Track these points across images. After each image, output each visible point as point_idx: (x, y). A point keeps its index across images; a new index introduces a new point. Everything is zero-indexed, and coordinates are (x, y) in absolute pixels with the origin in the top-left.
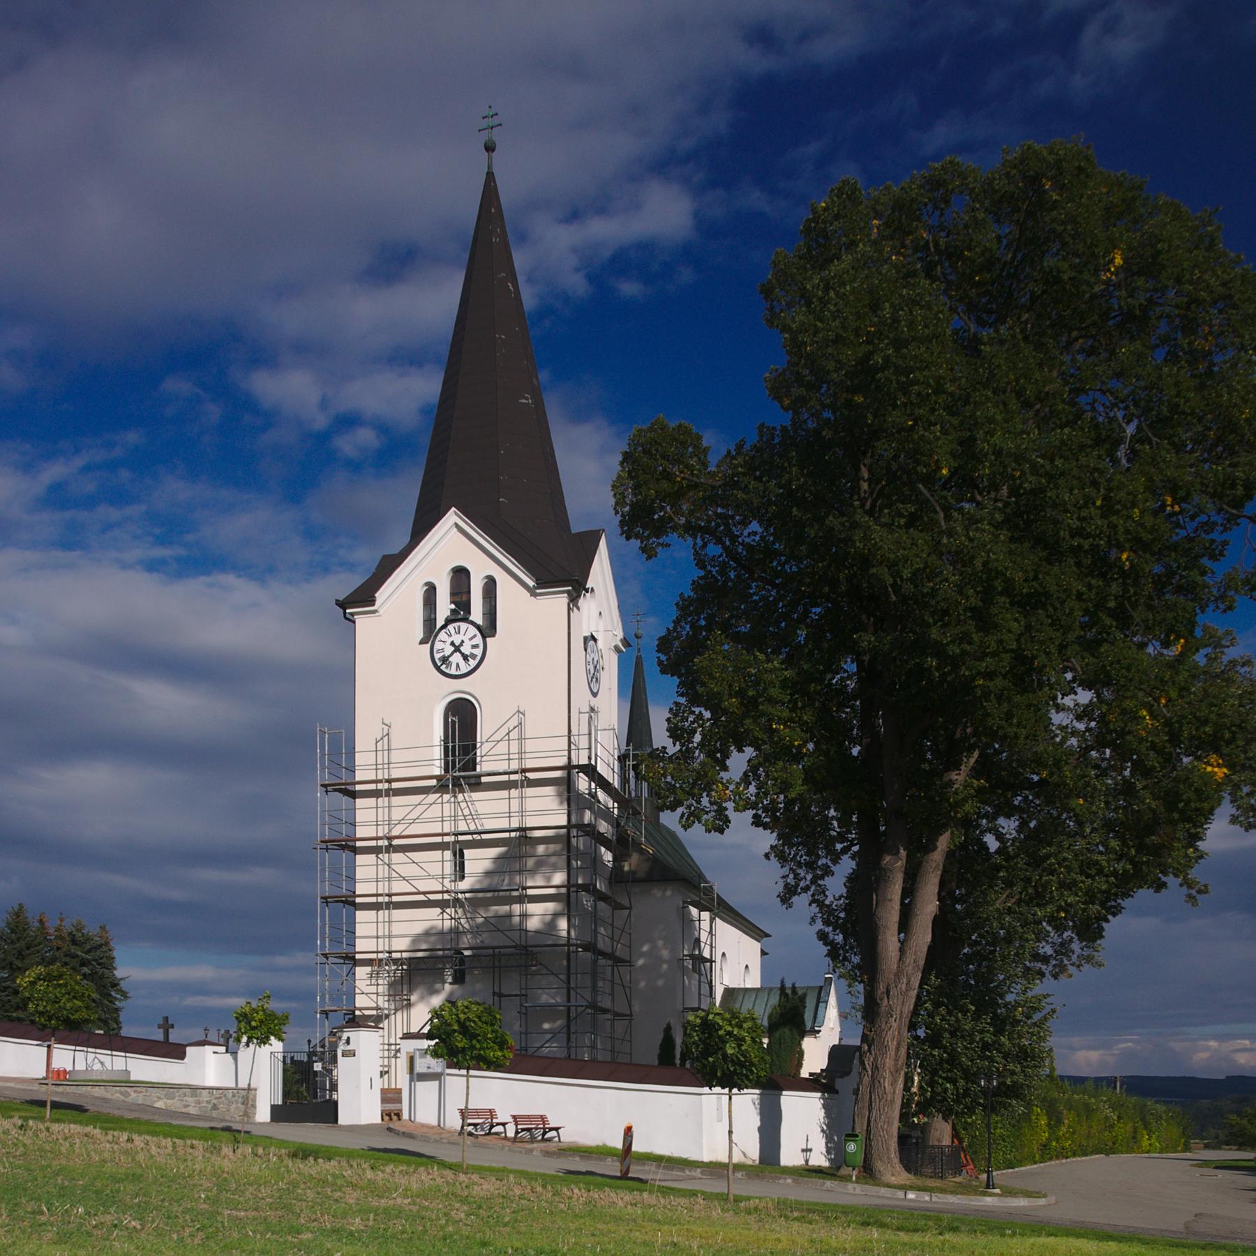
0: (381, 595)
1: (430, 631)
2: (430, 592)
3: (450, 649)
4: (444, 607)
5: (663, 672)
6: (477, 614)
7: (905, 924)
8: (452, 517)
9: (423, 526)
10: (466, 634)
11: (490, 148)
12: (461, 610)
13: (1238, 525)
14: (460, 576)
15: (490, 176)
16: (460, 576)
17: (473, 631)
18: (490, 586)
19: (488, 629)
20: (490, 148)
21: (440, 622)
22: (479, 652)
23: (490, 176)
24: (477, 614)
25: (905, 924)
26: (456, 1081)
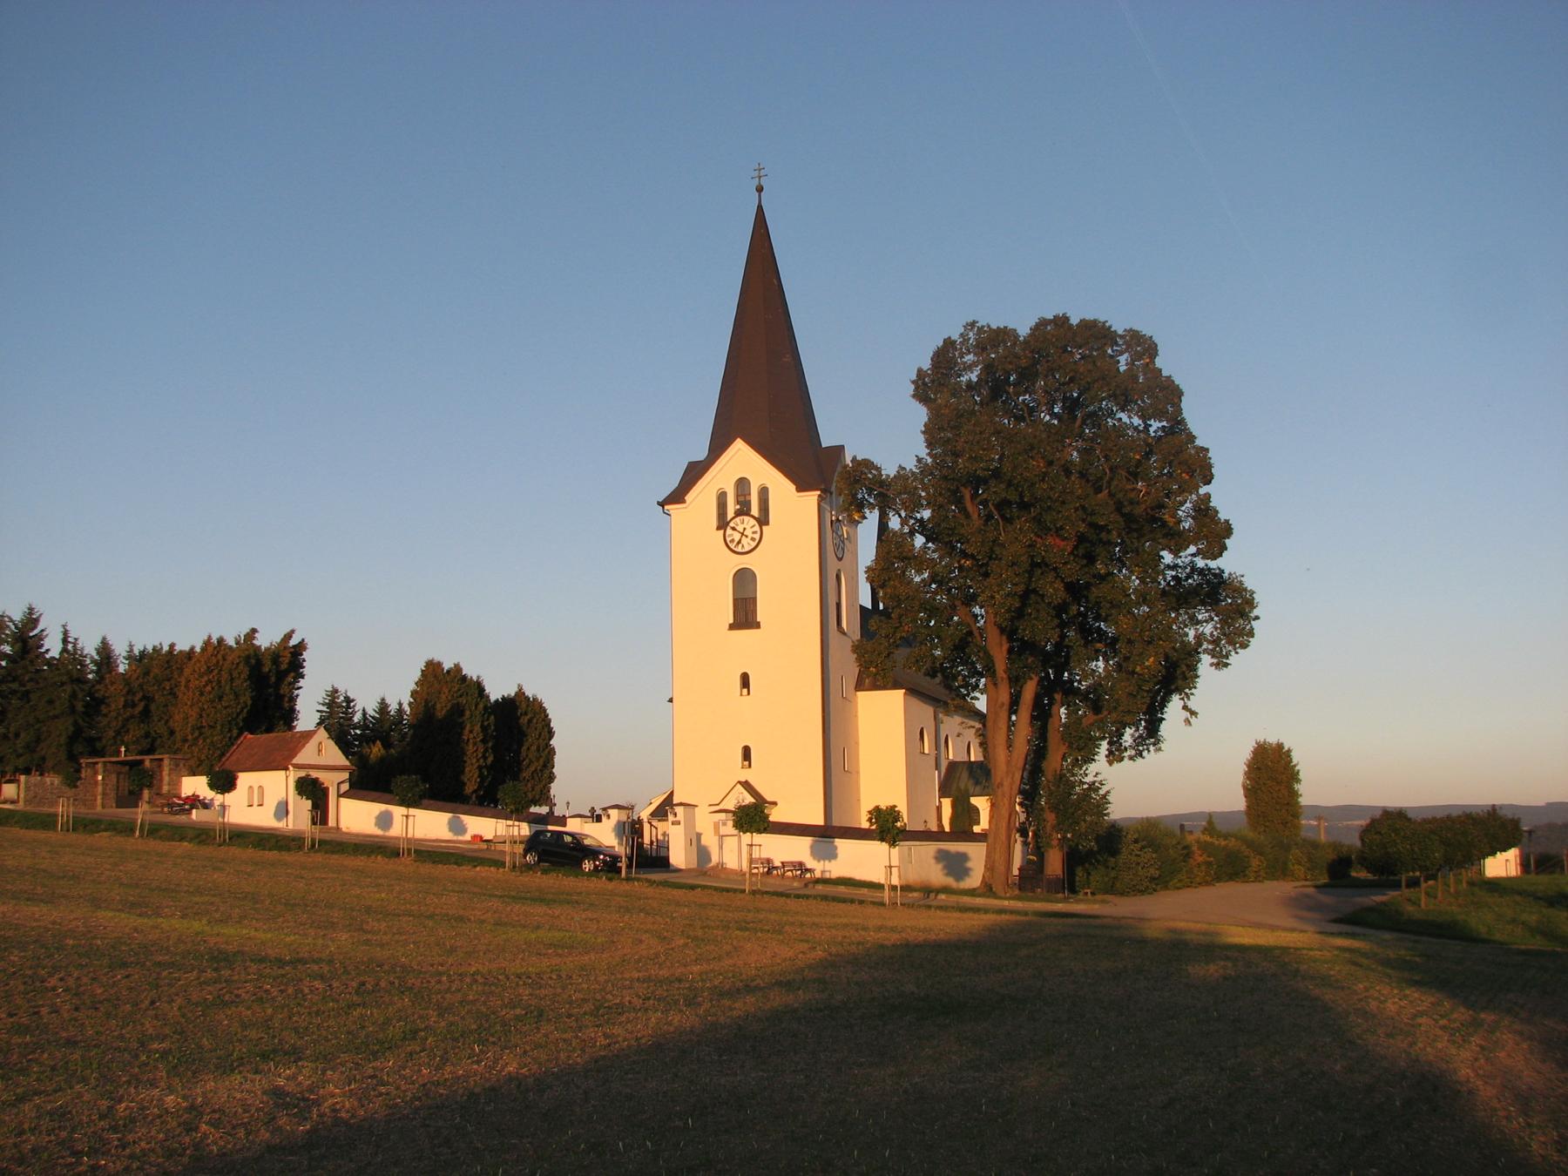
0: (689, 498)
1: (723, 524)
2: (722, 499)
3: (740, 528)
4: (731, 508)
5: (925, 388)
6: (755, 511)
7: (1010, 745)
8: (739, 445)
9: (718, 446)
10: (748, 524)
11: (760, 189)
12: (744, 510)
13: (1257, 618)
14: (742, 484)
15: (760, 208)
16: (742, 484)
17: (753, 522)
18: (764, 492)
19: (763, 520)
20: (760, 189)
21: (730, 514)
22: (757, 537)
23: (760, 208)
24: (755, 511)
25: (1010, 745)
26: (746, 838)
